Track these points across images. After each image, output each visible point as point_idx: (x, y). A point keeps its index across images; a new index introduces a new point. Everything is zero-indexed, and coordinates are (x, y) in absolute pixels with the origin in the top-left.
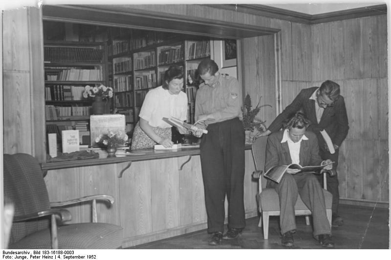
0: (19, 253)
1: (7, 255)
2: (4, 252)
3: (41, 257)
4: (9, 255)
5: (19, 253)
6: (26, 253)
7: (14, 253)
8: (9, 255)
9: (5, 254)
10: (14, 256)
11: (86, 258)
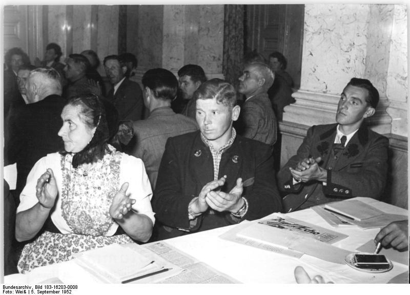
0: (20, 288)
1: (7, 290)
2: (4, 287)
3: (61, 293)
4: (10, 290)
6: (27, 288)
7: (14, 287)
8: (10, 290)
9: (5, 289)
10: (14, 290)
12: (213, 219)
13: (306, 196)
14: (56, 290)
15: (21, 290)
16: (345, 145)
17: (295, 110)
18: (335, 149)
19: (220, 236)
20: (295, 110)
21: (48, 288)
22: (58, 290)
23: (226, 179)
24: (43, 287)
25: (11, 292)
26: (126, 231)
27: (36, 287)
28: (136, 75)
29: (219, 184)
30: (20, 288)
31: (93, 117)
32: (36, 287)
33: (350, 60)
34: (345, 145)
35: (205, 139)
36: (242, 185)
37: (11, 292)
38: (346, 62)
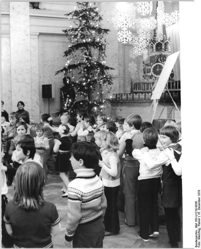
0: (197, 237)
1: (198, 245)
2: (196, 247)
4: (198, 243)
7: (196, 240)
8: (198, 243)
9: (197, 246)
13: (46, 92)
14: (198, 221)
16: (68, 151)
18: (77, 86)
19: (178, 161)
21: (196, 220)
22: (198, 219)
24: (196, 223)
27: (196, 227)
30: (197, 237)
31: (34, 174)
32: (196, 227)
33: (38, 8)
34: (68, 151)
35: (67, 100)
36: (168, 81)
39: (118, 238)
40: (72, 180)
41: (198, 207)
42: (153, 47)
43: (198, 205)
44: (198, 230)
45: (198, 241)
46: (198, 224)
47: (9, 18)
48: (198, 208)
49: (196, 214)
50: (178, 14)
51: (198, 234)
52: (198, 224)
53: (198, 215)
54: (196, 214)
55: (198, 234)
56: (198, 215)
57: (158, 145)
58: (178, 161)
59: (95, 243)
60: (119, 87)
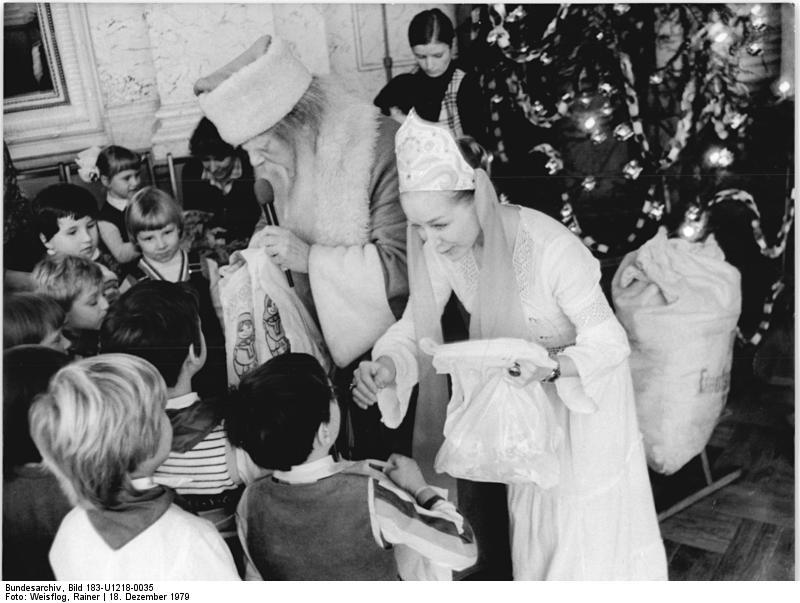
0: (39, 589)
1: (14, 593)
2: (8, 587)
4: (19, 593)
5: (39, 589)
7: (28, 588)
8: (19, 593)
11: (169, 597)
12: (90, 249)
14: (91, 593)
15: (41, 593)
17: (183, 122)
19: (453, 298)
20: (183, 122)
22: (96, 593)
23: (589, 135)
24: (85, 588)
25: (21, 598)
26: (365, 350)
27: (71, 587)
28: (165, 124)
29: (722, 131)
32: (71, 587)
37: (21, 598)
38: (192, 92)
39: (399, 526)
40: (794, 548)
41: (136, 593)
42: (708, 540)
43: (141, 593)
44: (60, 593)
45: (26, 592)
46: (81, 593)
47: (393, 318)
48: (133, 592)
49: (112, 588)
50: (102, 586)
51: (47, 593)
52: (81, 593)
53: (108, 594)
54: (112, 588)
55: (47, 593)
56: (108, 594)
57: (533, 369)
58: (453, 298)
59: (688, 538)
60: (721, 563)
